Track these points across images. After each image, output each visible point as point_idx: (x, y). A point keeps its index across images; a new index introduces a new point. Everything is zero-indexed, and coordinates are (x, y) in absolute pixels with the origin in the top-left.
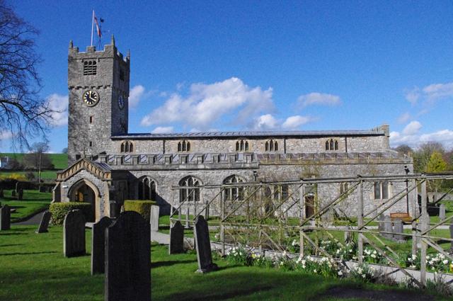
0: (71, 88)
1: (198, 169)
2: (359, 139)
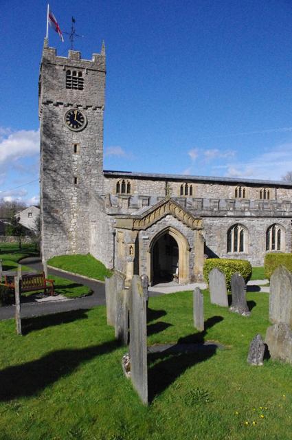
0: (49, 102)
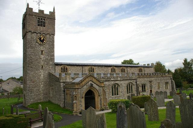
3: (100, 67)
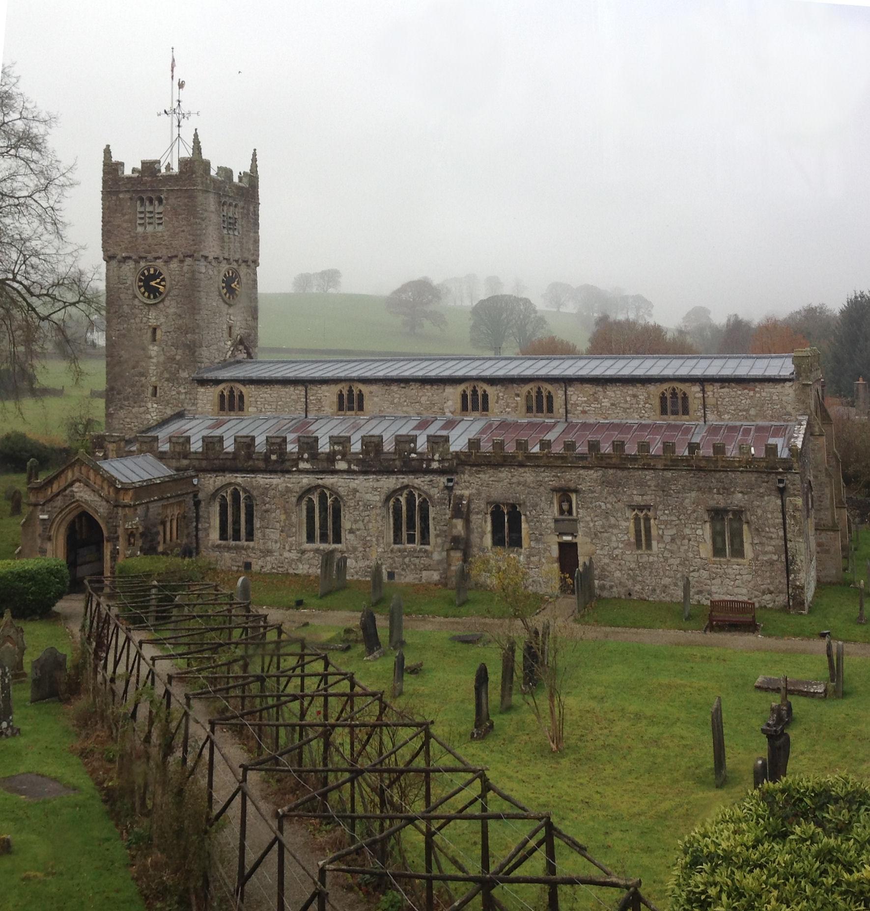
1: (788, 588)
2: (736, 391)
3: (394, 388)
